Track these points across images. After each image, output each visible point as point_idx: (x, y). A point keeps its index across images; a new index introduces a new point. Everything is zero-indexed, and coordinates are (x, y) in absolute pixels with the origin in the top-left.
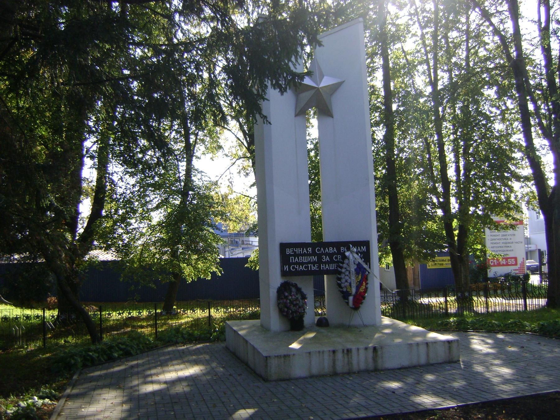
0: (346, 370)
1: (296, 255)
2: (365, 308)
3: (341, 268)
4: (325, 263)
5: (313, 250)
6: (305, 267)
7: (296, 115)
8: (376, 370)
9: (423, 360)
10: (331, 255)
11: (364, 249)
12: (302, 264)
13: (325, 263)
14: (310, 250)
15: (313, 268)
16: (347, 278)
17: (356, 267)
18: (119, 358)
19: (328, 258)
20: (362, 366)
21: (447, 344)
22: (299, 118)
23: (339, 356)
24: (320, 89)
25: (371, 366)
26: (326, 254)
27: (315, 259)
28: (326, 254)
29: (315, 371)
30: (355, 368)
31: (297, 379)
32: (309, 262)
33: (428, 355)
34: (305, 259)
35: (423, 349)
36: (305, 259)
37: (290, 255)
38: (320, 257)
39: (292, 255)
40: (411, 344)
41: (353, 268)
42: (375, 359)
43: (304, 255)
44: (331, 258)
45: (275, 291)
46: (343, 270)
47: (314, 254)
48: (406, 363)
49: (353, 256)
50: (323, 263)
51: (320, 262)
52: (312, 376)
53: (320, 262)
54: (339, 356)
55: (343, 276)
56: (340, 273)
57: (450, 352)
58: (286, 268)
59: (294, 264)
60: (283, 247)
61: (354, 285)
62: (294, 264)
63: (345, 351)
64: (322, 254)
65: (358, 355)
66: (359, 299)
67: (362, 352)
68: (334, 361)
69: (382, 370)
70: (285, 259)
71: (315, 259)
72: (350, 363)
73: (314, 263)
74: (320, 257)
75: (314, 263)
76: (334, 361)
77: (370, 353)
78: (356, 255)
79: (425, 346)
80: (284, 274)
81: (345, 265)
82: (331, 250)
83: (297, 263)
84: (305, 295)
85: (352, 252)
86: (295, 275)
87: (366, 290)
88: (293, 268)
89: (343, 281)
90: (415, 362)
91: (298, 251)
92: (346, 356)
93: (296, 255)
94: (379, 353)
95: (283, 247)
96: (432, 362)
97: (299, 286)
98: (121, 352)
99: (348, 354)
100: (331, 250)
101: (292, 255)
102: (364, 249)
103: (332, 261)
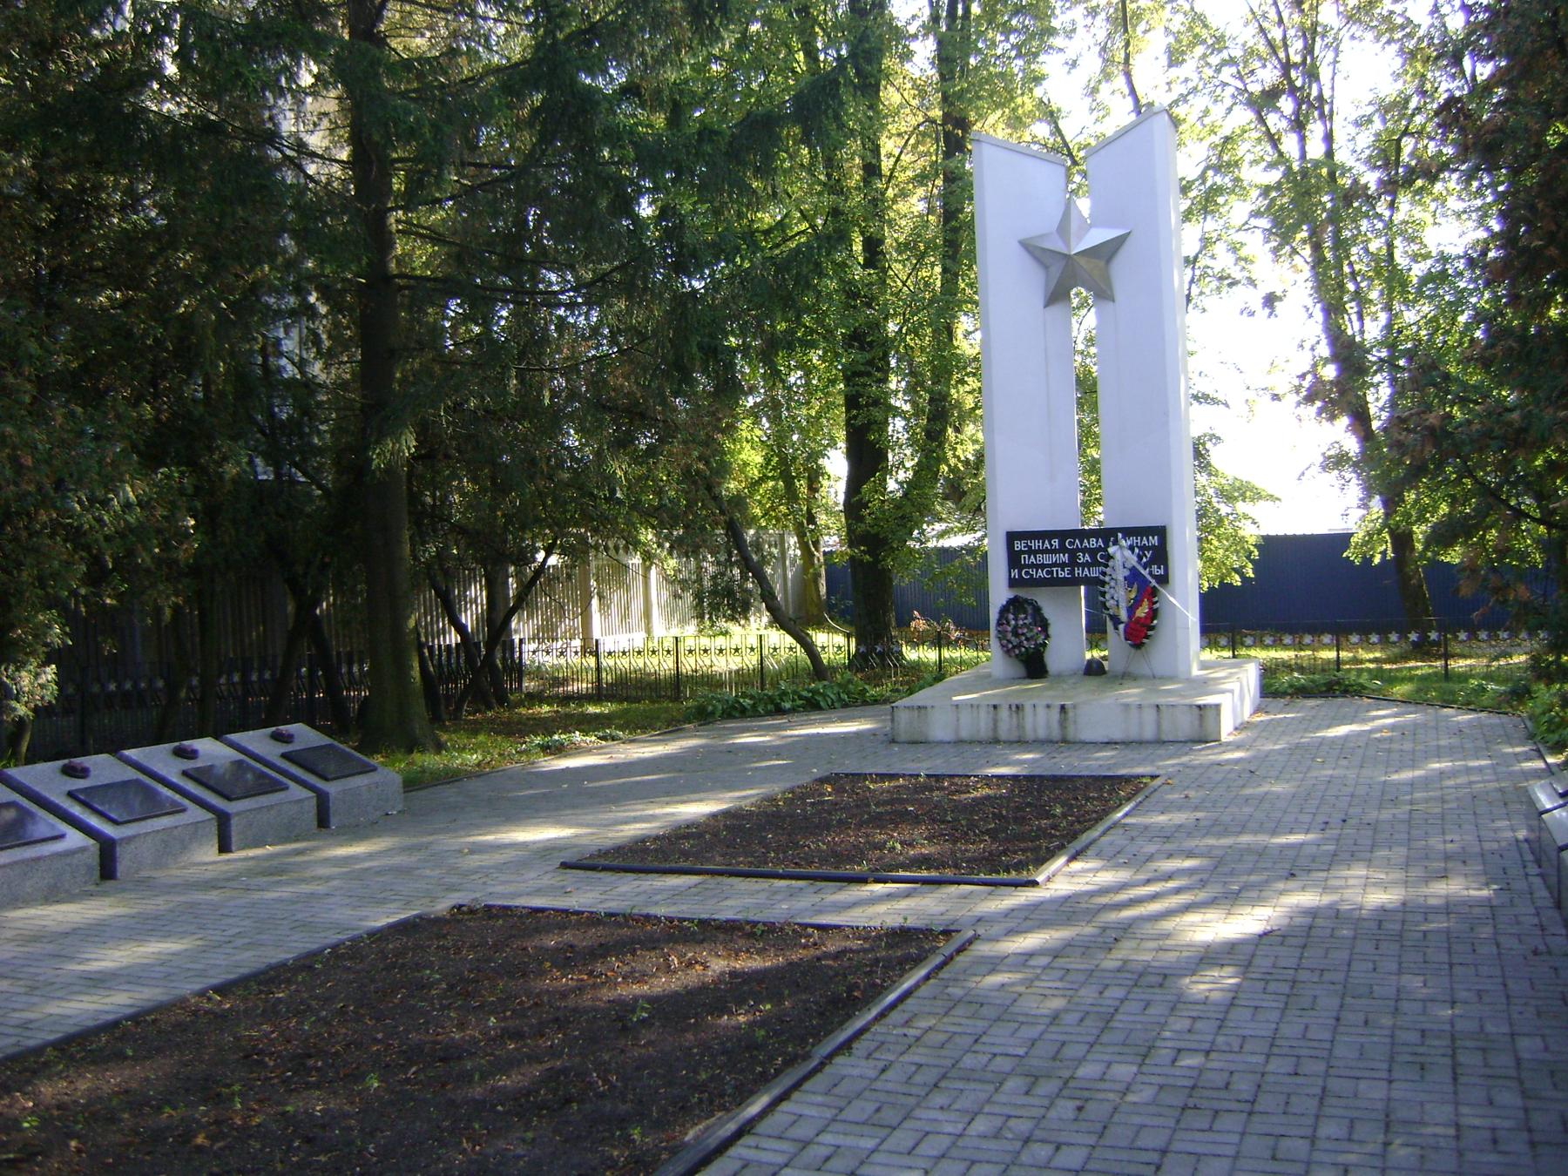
0: (1014, 736)
1: (1030, 552)
2: (1159, 652)
3: (1104, 574)
4: (1083, 565)
5: (1062, 544)
6: (1048, 573)
7: (1046, 306)
8: (1065, 741)
9: (1149, 733)
10: (1093, 552)
11: (1154, 541)
12: (1043, 566)
13: (1083, 565)
14: (1056, 543)
15: (1062, 574)
16: (1112, 591)
17: (1127, 573)
18: (793, 710)
19: (1087, 558)
20: (1042, 734)
21: (1196, 711)
22: (1056, 310)
23: (1004, 713)
24: (1082, 261)
25: (1056, 733)
26: (1084, 550)
27: (1065, 558)
28: (1084, 550)
29: (964, 734)
30: (1030, 735)
31: (941, 743)
32: (1055, 565)
33: (1159, 724)
34: (1047, 559)
35: (1149, 716)
36: (1047, 559)
37: (1022, 552)
38: (1073, 554)
39: (1024, 552)
40: (1127, 706)
41: (1121, 574)
42: (1063, 724)
43: (1046, 551)
44: (1093, 556)
45: (997, 610)
46: (1107, 579)
47: (1062, 549)
48: (1117, 735)
49: (1122, 555)
50: (1079, 565)
51: (1073, 563)
52: (959, 742)
53: (1073, 563)
54: (1004, 713)
55: (1107, 588)
56: (1103, 583)
57: (1201, 725)
58: (1015, 573)
59: (1028, 566)
60: (1012, 537)
61: (1123, 605)
62: (1028, 566)
63: (1014, 708)
64: (1078, 550)
65: (1035, 715)
66: (1140, 633)
67: (1041, 711)
68: (995, 722)
69: (1074, 743)
70: (1014, 559)
71: (1065, 558)
72: (1020, 726)
73: (1063, 566)
74: (1073, 554)
75: (1063, 566)
76: (995, 722)
77: (1055, 714)
78: (1128, 553)
79: (1154, 711)
80: (1013, 583)
81: (1108, 570)
82: (1093, 543)
83: (1032, 566)
84: (1233, 646)
85: (1121, 547)
86: (1031, 586)
87: (1154, 614)
88: (1027, 573)
89: (1107, 596)
90: (1133, 734)
91: (1035, 544)
92: (1014, 715)
93: (1030, 552)
94: (1071, 714)
95: (1012, 537)
96: (1165, 738)
97: (1048, 612)
98: (800, 702)
99: (1017, 712)
100: (1093, 543)
101: (1024, 552)
102: (1154, 541)
103: (1095, 563)
